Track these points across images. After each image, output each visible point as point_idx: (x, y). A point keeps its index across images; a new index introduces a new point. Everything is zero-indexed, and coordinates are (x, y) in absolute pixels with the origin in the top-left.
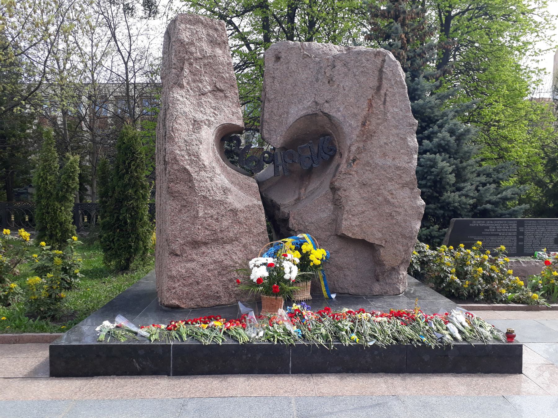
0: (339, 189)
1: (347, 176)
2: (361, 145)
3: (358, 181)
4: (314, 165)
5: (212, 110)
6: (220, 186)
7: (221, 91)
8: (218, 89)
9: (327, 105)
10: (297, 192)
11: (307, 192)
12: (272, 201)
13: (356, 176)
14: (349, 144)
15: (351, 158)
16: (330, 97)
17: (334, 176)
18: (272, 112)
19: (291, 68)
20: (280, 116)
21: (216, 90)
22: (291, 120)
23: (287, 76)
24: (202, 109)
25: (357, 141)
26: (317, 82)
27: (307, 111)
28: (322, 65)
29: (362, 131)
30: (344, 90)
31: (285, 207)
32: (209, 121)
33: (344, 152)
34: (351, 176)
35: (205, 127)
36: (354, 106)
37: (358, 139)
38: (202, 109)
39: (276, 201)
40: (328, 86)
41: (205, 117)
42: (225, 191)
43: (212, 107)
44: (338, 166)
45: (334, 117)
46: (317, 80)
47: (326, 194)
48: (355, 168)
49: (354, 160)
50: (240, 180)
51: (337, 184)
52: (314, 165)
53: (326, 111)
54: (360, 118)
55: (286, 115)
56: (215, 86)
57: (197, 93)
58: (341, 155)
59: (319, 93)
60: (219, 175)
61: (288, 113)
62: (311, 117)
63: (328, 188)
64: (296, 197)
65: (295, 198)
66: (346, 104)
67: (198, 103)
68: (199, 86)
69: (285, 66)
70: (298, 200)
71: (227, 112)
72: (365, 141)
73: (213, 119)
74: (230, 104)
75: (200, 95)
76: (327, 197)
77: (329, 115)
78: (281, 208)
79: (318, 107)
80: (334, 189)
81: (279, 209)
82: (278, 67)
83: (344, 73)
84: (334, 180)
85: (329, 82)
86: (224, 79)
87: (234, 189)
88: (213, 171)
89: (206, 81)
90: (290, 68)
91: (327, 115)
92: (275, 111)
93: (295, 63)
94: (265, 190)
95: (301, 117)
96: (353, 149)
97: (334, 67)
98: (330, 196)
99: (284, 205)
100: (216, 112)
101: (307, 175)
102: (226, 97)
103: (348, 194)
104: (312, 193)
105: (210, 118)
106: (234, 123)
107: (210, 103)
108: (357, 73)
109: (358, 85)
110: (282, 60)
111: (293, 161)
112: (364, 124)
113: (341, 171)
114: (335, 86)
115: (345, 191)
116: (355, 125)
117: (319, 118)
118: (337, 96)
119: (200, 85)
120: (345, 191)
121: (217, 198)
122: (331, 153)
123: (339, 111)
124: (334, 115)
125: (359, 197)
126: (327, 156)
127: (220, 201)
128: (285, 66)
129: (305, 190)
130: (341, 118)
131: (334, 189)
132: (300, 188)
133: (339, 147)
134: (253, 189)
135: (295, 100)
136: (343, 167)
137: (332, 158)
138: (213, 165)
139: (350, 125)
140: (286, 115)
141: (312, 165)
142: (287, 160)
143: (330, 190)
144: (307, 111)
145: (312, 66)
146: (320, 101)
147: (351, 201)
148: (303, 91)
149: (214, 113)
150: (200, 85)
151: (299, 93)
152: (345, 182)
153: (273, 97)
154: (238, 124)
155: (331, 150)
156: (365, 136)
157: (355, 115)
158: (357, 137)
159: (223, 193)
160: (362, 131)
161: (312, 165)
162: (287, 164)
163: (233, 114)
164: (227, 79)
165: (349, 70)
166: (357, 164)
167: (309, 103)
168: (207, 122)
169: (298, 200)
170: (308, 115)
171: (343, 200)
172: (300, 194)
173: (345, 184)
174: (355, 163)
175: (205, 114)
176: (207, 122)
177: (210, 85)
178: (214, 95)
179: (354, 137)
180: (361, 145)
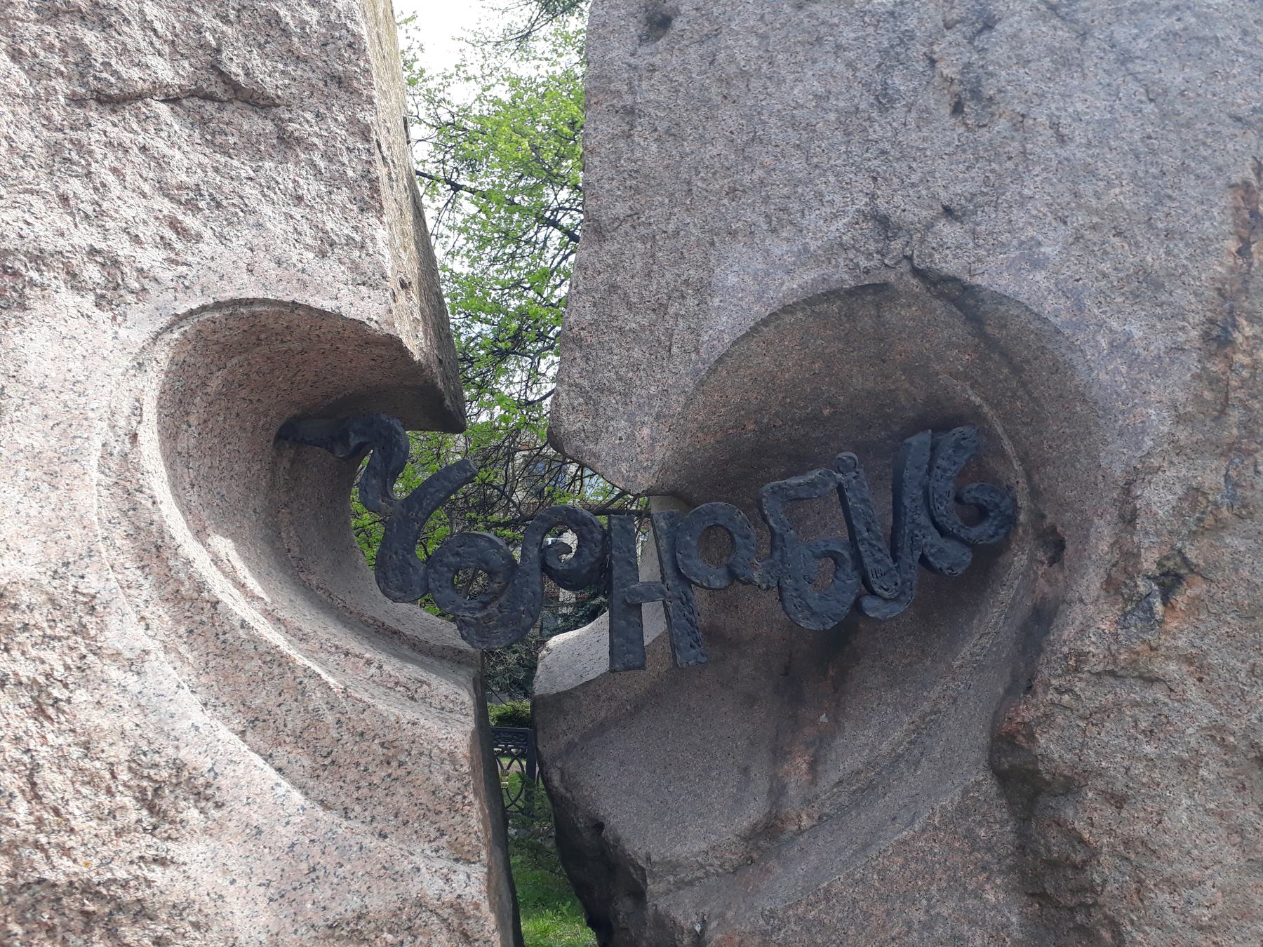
0: (1070, 787)
1: (1130, 692)
2: (1210, 475)
3: (1216, 733)
4: (868, 602)
5: (167, 207)
6: (121, 752)
7: (258, 101)
8: (235, 87)
9: (949, 231)
10: (761, 784)
11: (824, 784)
12: (599, 826)
13: (1194, 693)
14: (1118, 472)
15: (1149, 562)
16: (970, 188)
17: (1024, 684)
18: (613, 288)
19: (732, 59)
20: (660, 309)
21: (218, 90)
22: (724, 325)
23: (706, 102)
24: (74, 186)
25: (1179, 451)
26: (883, 109)
27: (826, 270)
28: (912, 23)
29: (1213, 381)
30: (1062, 140)
31: (681, 885)
32: (112, 263)
33: (1085, 528)
34: (1159, 693)
35: (66, 297)
36: (1139, 232)
37: (1182, 435)
38: (74, 186)
39: (625, 833)
40: (947, 131)
41: (85, 236)
42: (165, 791)
43: (163, 189)
44: (1041, 618)
45: (1001, 298)
46: (885, 100)
47: (963, 811)
48: (1179, 632)
49: (1169, 582)
50: (317, 699)
51: (1052, 747)
52: (868, 602)
53: (950, 265)
54: (1193, 303)
55: (691, 302)
56: (216, 68)
57: (60, 84)
58: (1055, 546)
59: (901, 167)
60: (135, 664)
61: (703, 289)
62: (851, 305)
63: (977, 775)
64: (754, 812)
65: (744, 823)
66: (1081, 218)
67: (54, 149)
68: (81, 46)
69: (693, 53)
70: (768, 835)
71: (277, 227)
72: (1231, 450)
73: (151, 257)
74: (311, 188)
75: (77, 101)
76: (970, 836)
77: (968, 289)
78: (653, 887)
79: (897, 245)
80: (1024, 784)
81: (639, 895)
82: (657, 60)
83: (1051, 51)
84: (1027, 713)
85: (957, 109)
86: (285, 32)
87: (259, 783)
88: (81, 630)
89: (147, 26)
90: (721, 57)
91: (958, 294)
92: (631, 286)
93: (751, 30)
94: (571, 746)
95: (787, 309)
96: (1158, 498)
97: (989, 25)
98: (997, 828)
99: (673, 866)
100: (191, 222)
101: (818, 669)
102: (287, 142)
103: (1142, 829)
104: (865, 789)
105: (122, 248)
106: (329, 305)
107: (161, 163)
108: (1142, 44)
109: (1149, 108)
110: (678, 24)
111: (732, 575)
112: (1218, 339)
113: (1081, 656)
114: (1002, 125)
115: (1119, 801)
116: (1160, 344)
117: (900, 315)
118: (1019, 178)
119: (90, 37)
120: (1119, 801)
121: (61, 870)
122: (982, 532)
123: (1037, 264)
124: (1004, 283)
125: (1231, 857)
126: (952, 548)
127: (88, 890)
128: (693, 53)
129: (813, 766)
130: (1054, 307)
131: (1024, 784)
132: (779, 754)
133: (1035, 493)
134: (420, 772)
135: (750, 217)
136: (1091, 622)
137: (987, 561)
138: (92, 583)
139: (1120, 346)
140: (691, 302)
141: (857, 607)
142: (696, 565)
143: (990, 786)
144: (826, 270)
145: (848, 35)
146: (906, 208)
147: (1172, 885)
148: (797, 164)
149: (174, 224)
150: (90, 37)
151: (777, 177)
152: (1111, 735)
153: (621, 209)
154: (352, 313)
155: (982, 513)
156: (1235, 415)
157: (1146, 285)
158: (1180, 419)
159: (134, 813)
160: (1213, 381)
161: (857, 607)
162: (699, 596)
163: (326, 246)
164: (304, 37)
165: (1084, 36)
166: (1196, 605)
167: (840, 224)
168: (92, 273)
169: (768, 835)
170: (831, 295)
171: (1109, 874)
172: (777, 792)
173: (1112, 749)
174: (1180, 600)
175: (96, 217)
176: (92, 273)
177: (175, 55)
178: (204, 122)
179: (1158, 420)
180: (1210, 475)
